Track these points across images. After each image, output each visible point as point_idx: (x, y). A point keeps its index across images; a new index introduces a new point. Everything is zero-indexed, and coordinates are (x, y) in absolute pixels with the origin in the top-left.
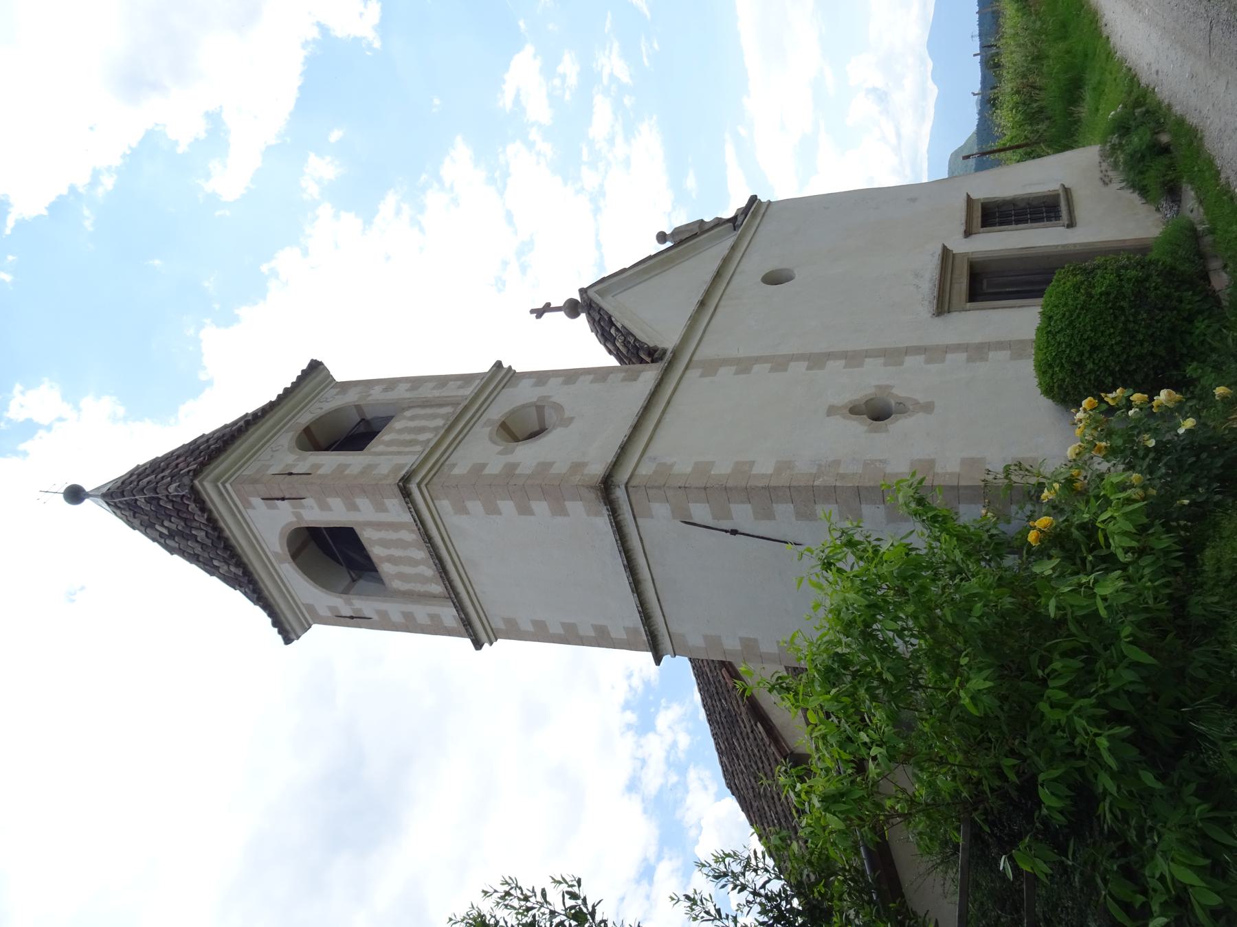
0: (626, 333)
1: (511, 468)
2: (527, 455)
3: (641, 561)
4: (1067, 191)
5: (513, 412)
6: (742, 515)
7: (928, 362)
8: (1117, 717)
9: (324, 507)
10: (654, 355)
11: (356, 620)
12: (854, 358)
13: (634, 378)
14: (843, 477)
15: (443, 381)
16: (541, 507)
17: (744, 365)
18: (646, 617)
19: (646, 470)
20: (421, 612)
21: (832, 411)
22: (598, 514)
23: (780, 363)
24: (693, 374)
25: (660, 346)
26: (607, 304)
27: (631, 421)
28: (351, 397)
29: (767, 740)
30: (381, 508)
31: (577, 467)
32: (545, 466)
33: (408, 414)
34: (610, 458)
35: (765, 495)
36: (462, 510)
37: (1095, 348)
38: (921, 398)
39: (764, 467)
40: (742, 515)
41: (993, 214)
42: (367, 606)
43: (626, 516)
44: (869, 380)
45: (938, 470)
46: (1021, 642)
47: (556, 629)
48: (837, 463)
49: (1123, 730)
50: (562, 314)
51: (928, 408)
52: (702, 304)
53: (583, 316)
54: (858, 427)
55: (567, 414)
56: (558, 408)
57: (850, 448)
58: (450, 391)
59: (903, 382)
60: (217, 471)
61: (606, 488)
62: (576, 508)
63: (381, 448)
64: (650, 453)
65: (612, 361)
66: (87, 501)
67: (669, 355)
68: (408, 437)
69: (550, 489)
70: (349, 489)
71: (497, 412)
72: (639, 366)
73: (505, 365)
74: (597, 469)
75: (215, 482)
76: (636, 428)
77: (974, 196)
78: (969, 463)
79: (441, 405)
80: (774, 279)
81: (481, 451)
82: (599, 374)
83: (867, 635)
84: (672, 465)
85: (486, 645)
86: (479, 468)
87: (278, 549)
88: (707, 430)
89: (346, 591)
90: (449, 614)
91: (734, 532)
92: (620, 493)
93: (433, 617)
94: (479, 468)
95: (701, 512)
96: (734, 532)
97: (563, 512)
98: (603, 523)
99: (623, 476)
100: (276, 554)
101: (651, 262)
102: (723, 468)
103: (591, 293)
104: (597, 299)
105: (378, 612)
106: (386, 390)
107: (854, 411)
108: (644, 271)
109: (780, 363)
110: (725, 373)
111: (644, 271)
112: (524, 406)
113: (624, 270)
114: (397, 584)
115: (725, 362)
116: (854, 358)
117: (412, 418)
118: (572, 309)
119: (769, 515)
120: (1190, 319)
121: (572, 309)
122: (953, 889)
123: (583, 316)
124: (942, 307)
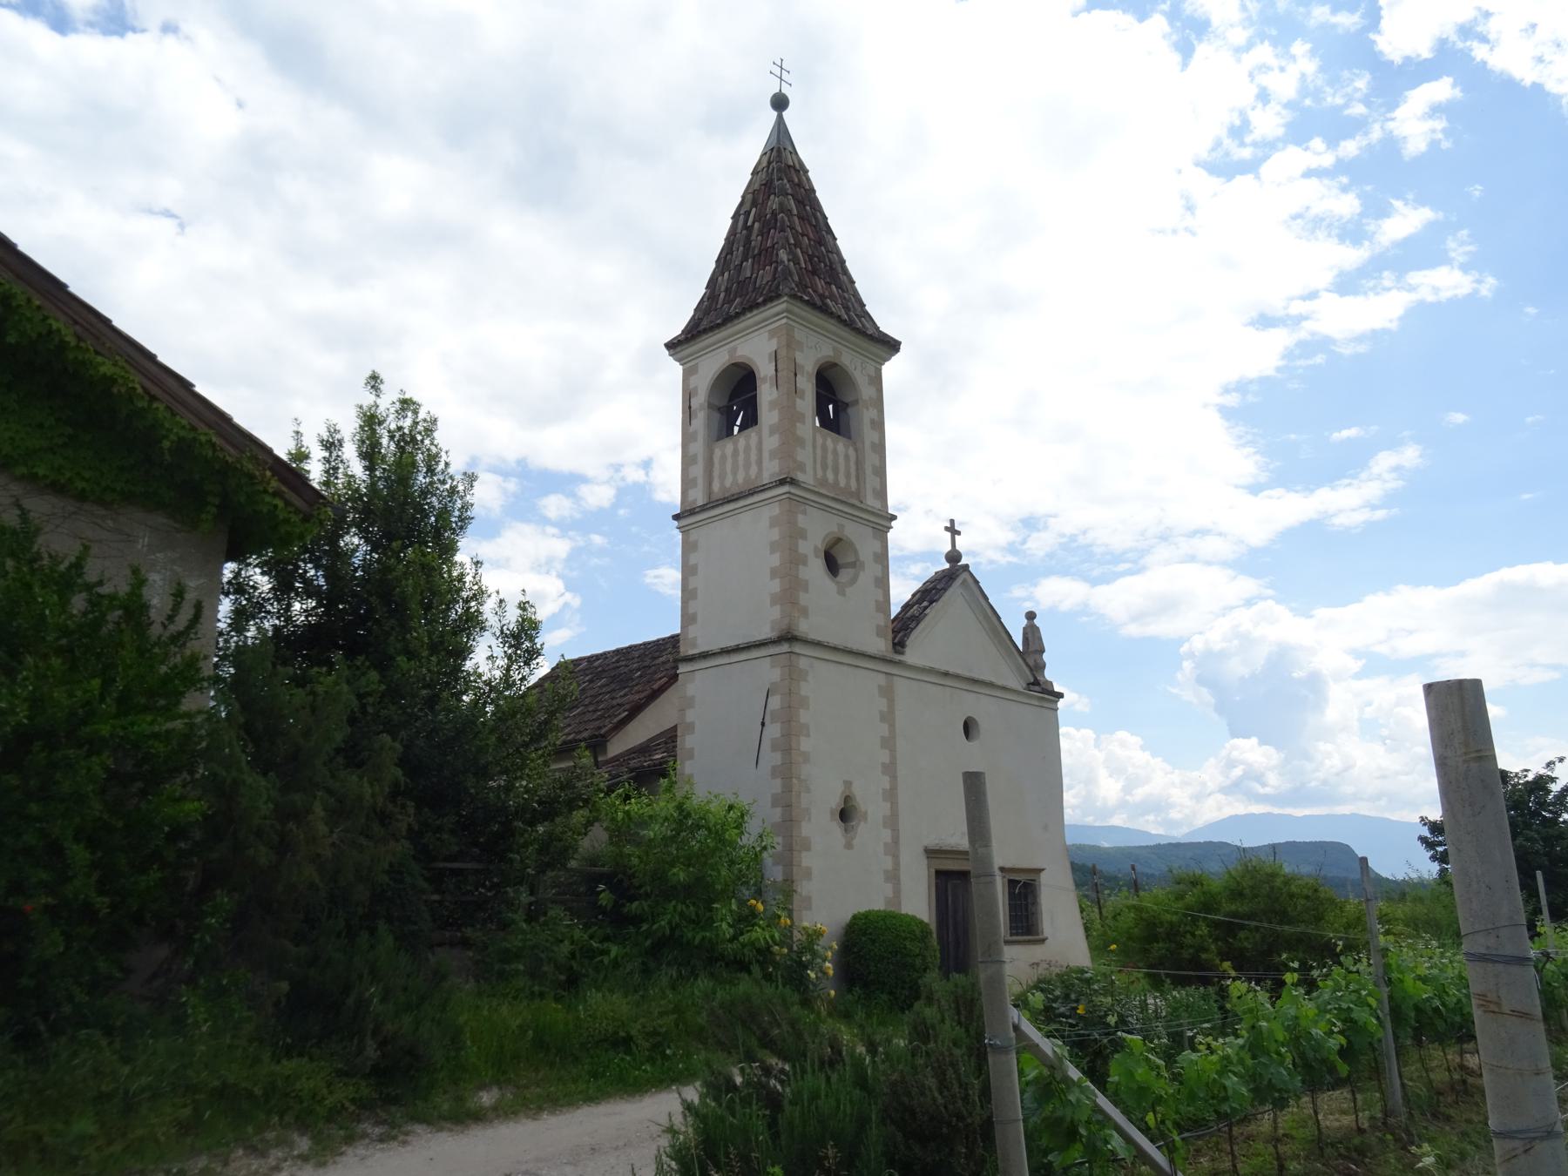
0: (917, 619)
1: (803, 560)
2: (815, 568)
4: (1043, 941)
5: (851, 544)
6: (774, 731)
7: (886, 844)
8: (672, 929)
9: (773, 405)
10: (899, 645)
11: (688, 412)
12: (891, 795)
13: (880, 632)
15: (881, 472)
16: (775, 586)
17: (888, 717)
19: (803, 663)
20: (698, 471)
21: (848, 784)
22: (773, 629)
23: (889, 743)
24: (882, 680)
25: (907, 650)
26: (955, 591)
28: (866, 392)
30: (773, 454)
31: (805, 612)
32: (805, 586)
33: (851, 451)
35: (786, 746)
36: (774, 523)
37: (874, 941)
38: (855, 842)
39: (805, 744)
41: (1023, 892)
42: (700, 421)
44: (872, 806)
46: (701, 893)
47: (692, 561)
48: (808, 791)
49: (668, 932)
50: (949, 548)
51: (849, 846)
52: (946, 674)
53: (947, 566)
54: (835, 802)
55: (848, 590)
56: (854, 580)
57: (822, 797)
58: (871, 481)
59: (871, 833)
60: (796, 310)
61: (788, 637)
62: (775, 613)
63: (820, 441)
64: (817, 663)
65: (895, 610)
66: (775, 114)
67: (898, 657)
69: (791, 593)
70: (791, 417)
71: (852, 531)
72: (890, 636)
74: (804, 628)
75: (787, 311)
76: (835, 649)
77: (1043, 875)
78: (808, 874)
80: (969, 728)
81: (817, 528)
83: (699, 827)
85: (676, 523)
86: (802, 534)
87: (739, 353)
88: (838, 701)
89: (710, 406)
90: (699, 498)
91: (763, 724)
92: (785, 647)
93: (695, 480)
94: (802, 534)
96: (763, 724)
97: (773, 603)
98: (766, 633)
99: (798, 648)
100: (735, 349)
102: (804, 716)
103: (964, 575)
104: (959, 581)
105: (695, 432)
106: (873, 422)
107: (847, 799)
109: (889, 743)
110: (882, 704)
111: (986, 616)
112: (856, 552)
113: (986, 599)
114: (717, 453)
116: (891, 795)
117: (847, 457)
118: (953, 557)
119: (774, 748)
120: (891, 993)
121: (953, 557)
122: (767, 874)
123: (947, 566)
124: (932, 853)
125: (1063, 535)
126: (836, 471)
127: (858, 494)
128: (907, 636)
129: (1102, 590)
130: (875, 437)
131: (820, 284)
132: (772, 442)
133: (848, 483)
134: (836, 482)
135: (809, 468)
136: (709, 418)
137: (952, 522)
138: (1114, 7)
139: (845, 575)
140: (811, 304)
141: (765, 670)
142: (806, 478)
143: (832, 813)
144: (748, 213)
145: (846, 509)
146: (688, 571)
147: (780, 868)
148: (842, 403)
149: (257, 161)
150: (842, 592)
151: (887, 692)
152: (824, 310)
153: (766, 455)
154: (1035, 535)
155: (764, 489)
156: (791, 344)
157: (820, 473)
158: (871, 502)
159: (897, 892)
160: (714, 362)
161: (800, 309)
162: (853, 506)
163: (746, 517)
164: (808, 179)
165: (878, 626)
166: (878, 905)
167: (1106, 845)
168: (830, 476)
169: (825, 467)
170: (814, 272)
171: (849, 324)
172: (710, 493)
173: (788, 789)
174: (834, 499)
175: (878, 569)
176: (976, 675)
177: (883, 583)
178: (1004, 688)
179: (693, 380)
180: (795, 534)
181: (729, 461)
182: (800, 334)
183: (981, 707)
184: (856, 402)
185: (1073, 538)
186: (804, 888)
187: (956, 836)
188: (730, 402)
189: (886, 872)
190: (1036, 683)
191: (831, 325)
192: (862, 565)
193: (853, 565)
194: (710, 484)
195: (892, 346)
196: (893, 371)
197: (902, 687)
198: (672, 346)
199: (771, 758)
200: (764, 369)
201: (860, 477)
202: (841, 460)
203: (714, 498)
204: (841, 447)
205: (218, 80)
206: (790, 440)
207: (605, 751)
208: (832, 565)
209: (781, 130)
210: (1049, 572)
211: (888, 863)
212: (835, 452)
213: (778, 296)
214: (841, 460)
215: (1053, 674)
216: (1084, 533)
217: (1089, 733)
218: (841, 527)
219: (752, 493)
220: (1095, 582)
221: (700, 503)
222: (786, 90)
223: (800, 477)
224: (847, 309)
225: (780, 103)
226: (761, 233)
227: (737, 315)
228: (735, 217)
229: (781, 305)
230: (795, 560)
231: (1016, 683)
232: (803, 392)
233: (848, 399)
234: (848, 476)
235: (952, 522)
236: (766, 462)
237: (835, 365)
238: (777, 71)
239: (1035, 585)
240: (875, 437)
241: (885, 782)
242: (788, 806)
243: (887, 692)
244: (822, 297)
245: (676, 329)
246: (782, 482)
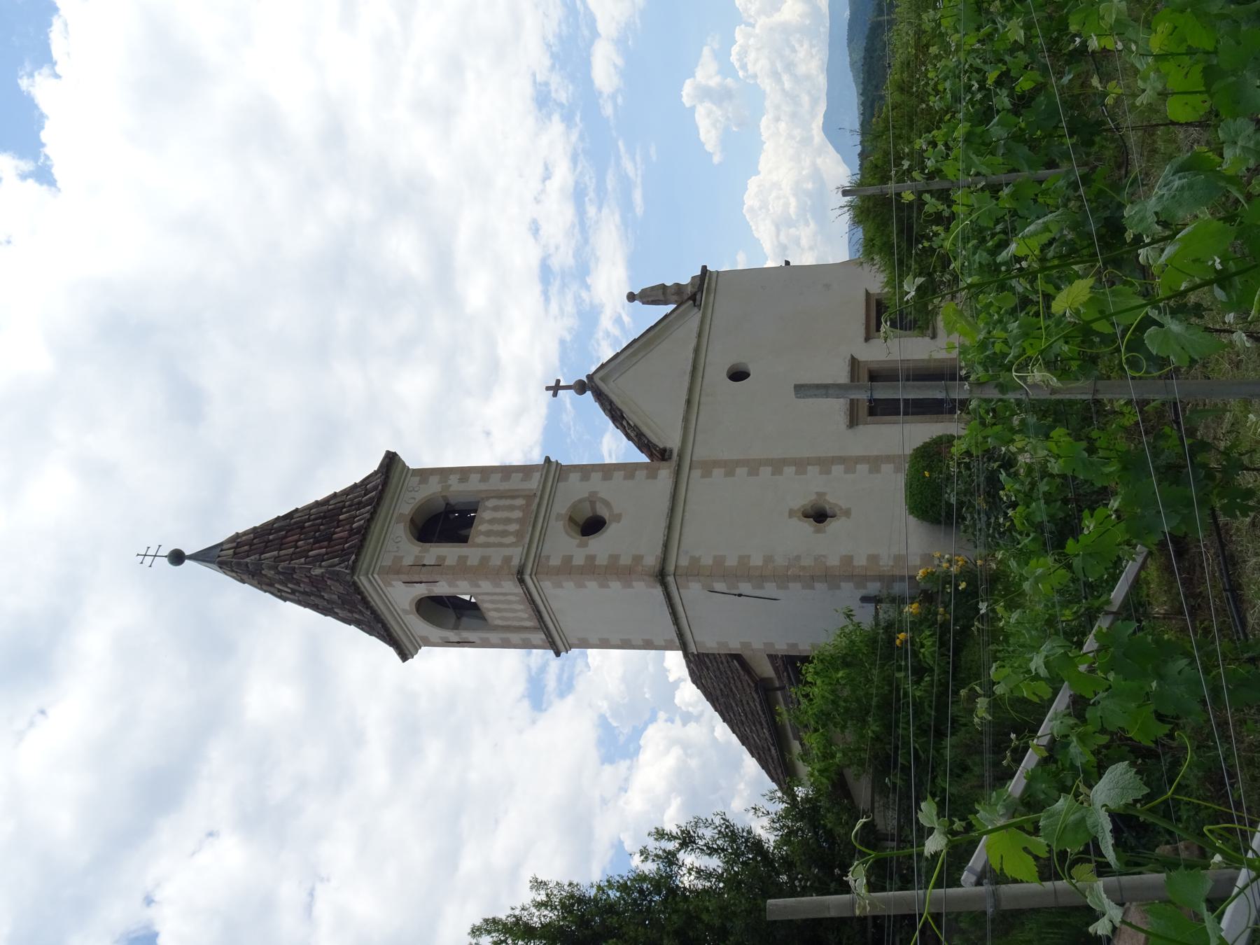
1: (591, 558)
2: (598, 545)
3: (680, 609)
5: (574, 507)
6: (745, 588)
7: (846, 472)
9: (451, 585)
12: (801, 465)
14: (804, 568)
17: (730, 467)
18: (681, 635)
19: (684, 562)
20: (515, 637)
23: (753, 466)
24: (696, 473)
25: (668, 446)
27: (663, 524)
28: (433, 488)
29: (742, 672)
31: (638, 559)
33: (490, 503)
34: (659, 551)
35: (760, 578)
40: (745, 588)
42: (467, 635)
43: (673, 588)
45: (855, 563)
48: (798, 558)
50: (572, 392)
52: (689, 402)
53: (589, 393)
54: (808, 526)
55: (616, 511)
58: (515, 483)
59: (835, 488)
60: (365, 566)
68: (500, 528)
70: (462, 570)
71: (562, 506)
73: (553, 459)
74: (651, 560)
76: (670, 527)
77: (871, 292)
79: (513, 497)
80: (738, 375)
81: (562, 544)
82: (628, 469)
84: (700, 558)
85: (563, 654)
86: (568, 559)
89: (456, 627)
90: (539, 637)
91: (740, 595)
92: (670, 579)
93: (523, 640)
94: (568, 559)
95: (719, 586)
96: (740, 595)
97: (630, 586)
98: (658, 591)
99: (671, 568)
100: (404, 611)
101: (636, 346)
103: (597, 379)
105: (481, 639)
107: (806, 516)
108: (634, 354)
109: (753, 466)
111: (634, 354)
112: (580, 501)
115: (716, 464)
116: (801, 465)
117: (496, 509)
118: (580, 387)
119: (762, 587)
121: (580, 387)
125: (553, 67)
126: (508, 521)
127: (529, 497)
128: (655, 446)
129: (601, 27)
130: (475, 478)
131: (340, 534)
132: (486, 586)
133: (519, 508)
134: (517, 520)
135: (507, 552)
136: (466, 629)
137: (548, 388)
138: (47, 38)
139: (603, 512)
140: (359, 548)
141: (692, 594)
142: (516, 554)
143: (818, 531)
144: (279, 590)
145: (545, 502)
146: (605, 644)
147: (869, 584)
148: (448, 514)
149: (264, 820)
150: (618, 518)
151: (708, 467)
152: (364, 533)
153: (498, 590)
154: (553, 95)
155: (528, 593)
156: (396, 570)
157: (511, 539)
158: (534, 483)
159: (888, 459)
160: (419, 626)
161: (364, 563)
162: (539, 505)
163: (555, 605)
164: (245, 533)
165: (648, 478)
166: (900, 481)
167: (847, 13)
168: (514, 527)
169: (504, 534)
170: (330, 539)
171: (377, 502)
172: (534, 629)
173: (797, 578)
174: (534, 527)
175: (596, 477)
176: (689, 368)
177: (607, 470)
178: (700, 335)
179: (432, 639)
180: (567, 569)
181: (505, 614)
182: (387, 561)
183: (717, 364)
184: (445, 498)
185: (554, 56)
186: (886, 564)
187: (837, 407)
188: (454, 617)
189: (871, 472)
190: (693, 298)
191: (376, 528)
192: (593, 494)
193: (593, 503)
194: (526, 628)
195: (391, 460)
196: (416, 458)
197: (702, 452)
198: (404, 656)
199: (770, 589)
200: (421, 590)
201: (512, 495)
202: (499, 515)
203: (537, 624)
204: (487, 515)
205: (193, 854)
206: (482, 570)
207: (770, 679)
208: (592, 526)
209: (203, 557)
210: (589, 81)
211: (863, 468)
212: (492, 521)
213: (355, 583)
214: (499, 515)
215: (685, 276)
216: (549, 46)
217: (739, 34)
218: (559, 517)
219: (532, 602)
220: (595, 34)
221: (543, 636)
222: (166, 551)
223: (516, 562)
224: (360, 505)
225: (177, 557)
226: (298, 584)
227: (374, 612)
228: (285, 599)
229: (363, 581)
230: (591, 569)
231: (694, 318)
232: (439, 557)
233: (443, 504)
234: (511, 508)
235: (548, 388)
236: (503, 591)
237: (412, 520)
238: (148, 560)
239: (600, 93)
240: (475, 478)
241: (789, 470)
242: (813, 578)
243: (708, 467)
244: (352, 532)
245: (390, 652)
246: (522, 581)
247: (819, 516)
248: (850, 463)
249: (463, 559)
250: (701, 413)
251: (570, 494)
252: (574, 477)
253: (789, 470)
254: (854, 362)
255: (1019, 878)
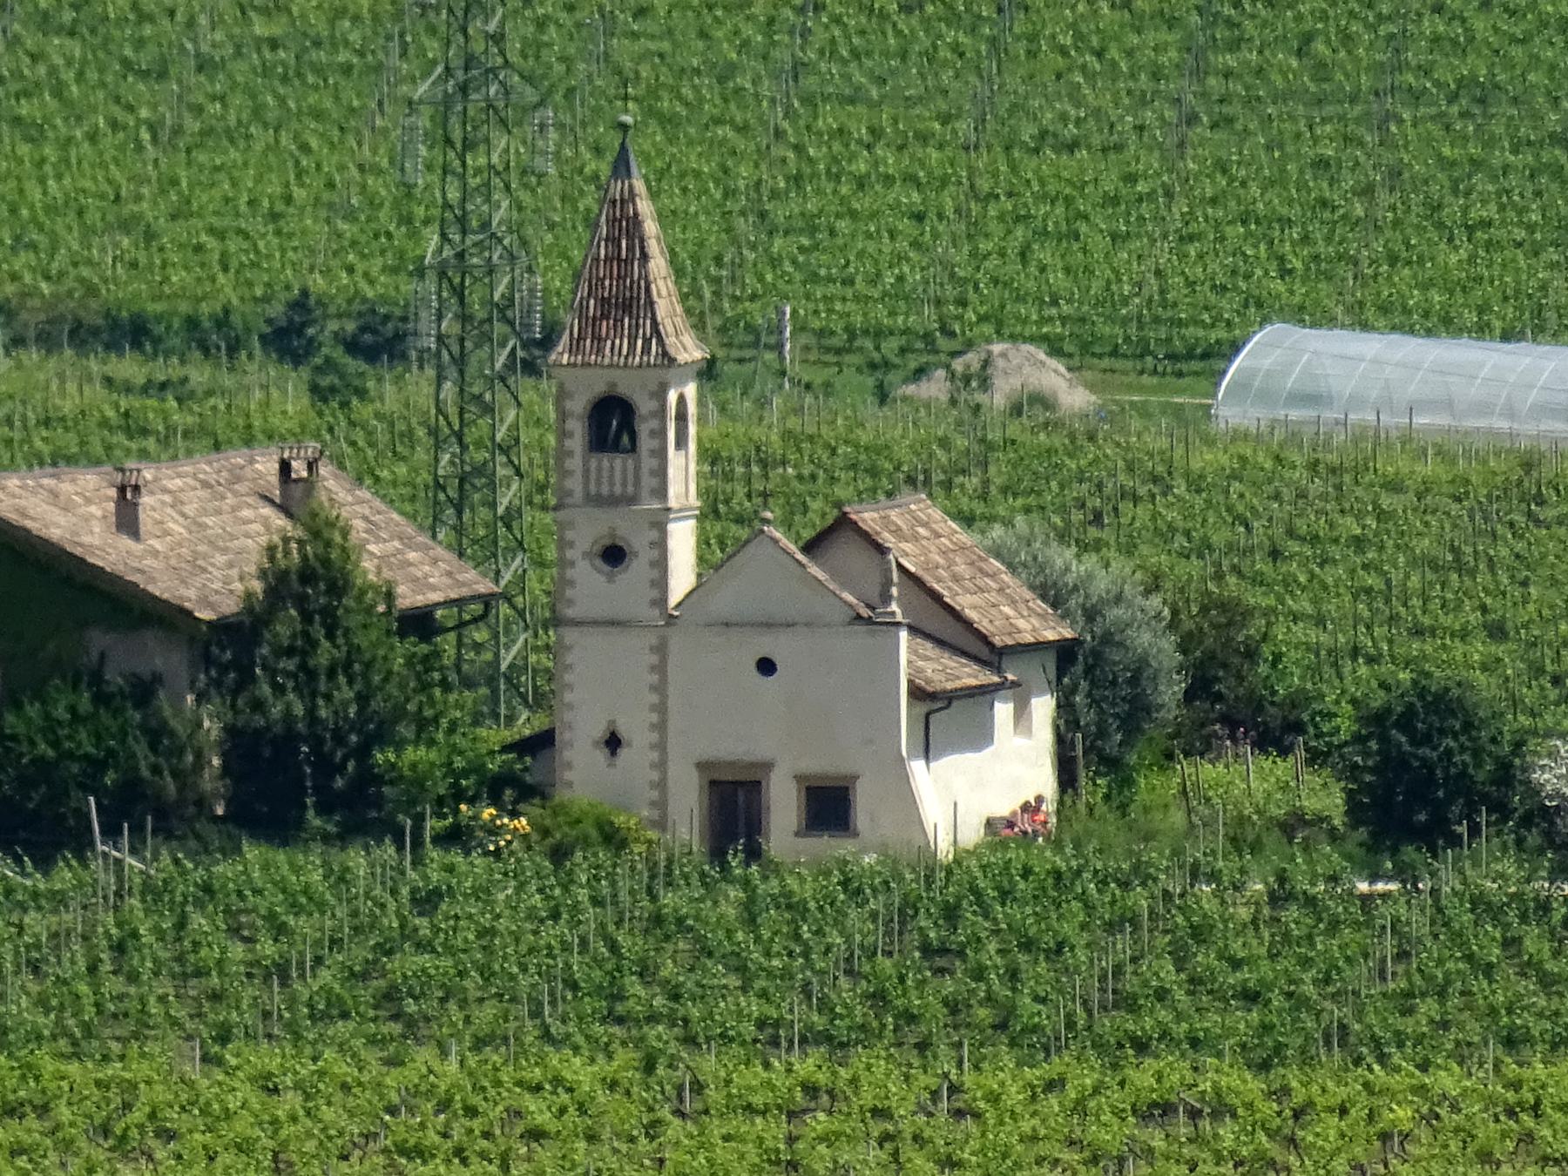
54: (623, 753)
59: (638, 755)
80: (766, 666)
86: (571, 544)
143: (629, 745)
208: (614, 555)
241: (654, 659)
247: (613, 742)
248: (661, 765)
249: (570, 454)
250: (788, 560)
251: (638, 541)
252: (654, 535)
253: (654, 659)
254: (767, 766)
255: (294, 510)
